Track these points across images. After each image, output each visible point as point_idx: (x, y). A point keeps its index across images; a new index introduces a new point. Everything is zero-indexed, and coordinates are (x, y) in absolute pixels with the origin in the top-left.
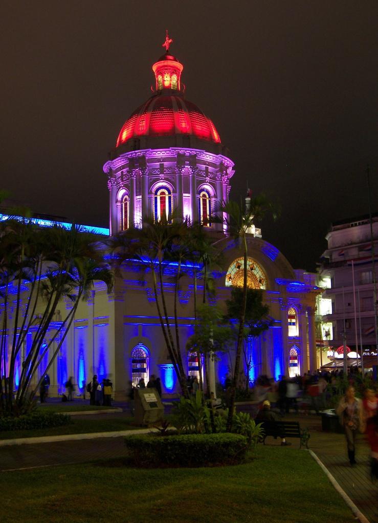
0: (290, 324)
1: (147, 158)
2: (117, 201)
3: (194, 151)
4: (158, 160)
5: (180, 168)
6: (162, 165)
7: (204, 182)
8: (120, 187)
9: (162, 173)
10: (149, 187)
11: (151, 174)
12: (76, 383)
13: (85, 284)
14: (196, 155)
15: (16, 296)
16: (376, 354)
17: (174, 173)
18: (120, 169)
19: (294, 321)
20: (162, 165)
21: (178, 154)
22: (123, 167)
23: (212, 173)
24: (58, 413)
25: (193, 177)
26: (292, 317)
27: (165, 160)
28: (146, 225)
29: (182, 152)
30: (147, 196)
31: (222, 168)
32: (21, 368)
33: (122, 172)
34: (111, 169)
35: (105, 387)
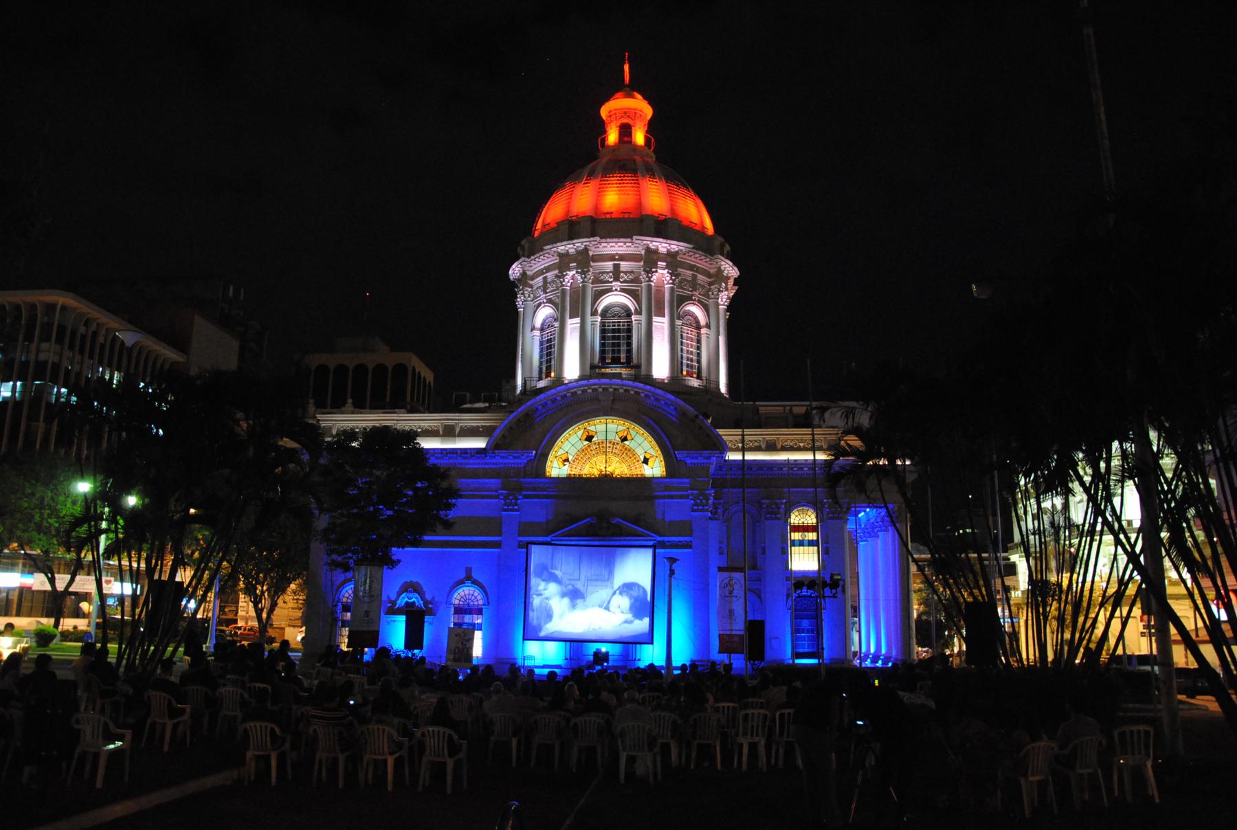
0: (793, 543)
1: (591, 253)
2: (533, 329)
4: (611, 258)
6: (617, 267)
8: (539, 305)
9: (617, 279)
10: (593, 304)
11: (597, 281)
14: (586, 250)
15: (647, 620)
16: (344, 648)
18: (541, 272)
20: (617, 267)
21: (648, 250)
25: (672, 290)
27: (623, 257)
29: (653, 245)
30: (589, 319)
32: (1055, 623)
33: (545, 278)
35: (550, 628)
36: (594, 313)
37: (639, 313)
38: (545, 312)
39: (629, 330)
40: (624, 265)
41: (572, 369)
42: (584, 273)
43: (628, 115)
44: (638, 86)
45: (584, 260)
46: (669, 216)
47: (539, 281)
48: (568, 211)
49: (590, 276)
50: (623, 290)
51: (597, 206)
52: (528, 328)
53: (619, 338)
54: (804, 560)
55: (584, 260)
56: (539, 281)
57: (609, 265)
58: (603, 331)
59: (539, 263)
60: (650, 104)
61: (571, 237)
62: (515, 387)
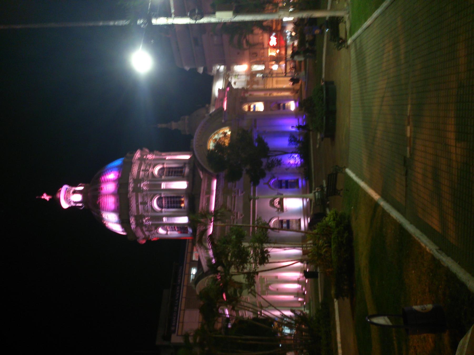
3: (131, 181)
4: (137, 206)
5: (143, 191)
6: (141, 203)
7: (152, 173)
12: (189, 250)
13: (263, 258)
14: (134, 179)
17: (147, 195)
19: (252, 106)
20: (141, 203)
21: (133, 191)
22: (142, 230)
23: (146, 167)
24: (277, 313)
26: (249, 108)
27: (137, 201)
28: (305, 262)
30: (163, 214)
31: (142, 160)
33: (146, 231)
34: (144, 239)
36: (161, 212)
37: (161, 194)
38: (161, 231)
39: (168, 197)
40: (140, 200)
41: (184, 220)
42: (144, 217)
43: (70, 197)
44: (54, 192)
45: (138, 180)
46: (117, 183)
47: (147, 233)
48: (117, 223)
49: (145, 214)
50: (154, 168)
51: (113, 194)
52: (167, 236)
53: (171, 201)
54: (260, 107)
55: (138, 180)
56: (147, 233)
57: (140, 207)
58: (168, 208)
59: (140, 234)
60: (62, 187)
61: (127, 184)
62: (227, 99)
